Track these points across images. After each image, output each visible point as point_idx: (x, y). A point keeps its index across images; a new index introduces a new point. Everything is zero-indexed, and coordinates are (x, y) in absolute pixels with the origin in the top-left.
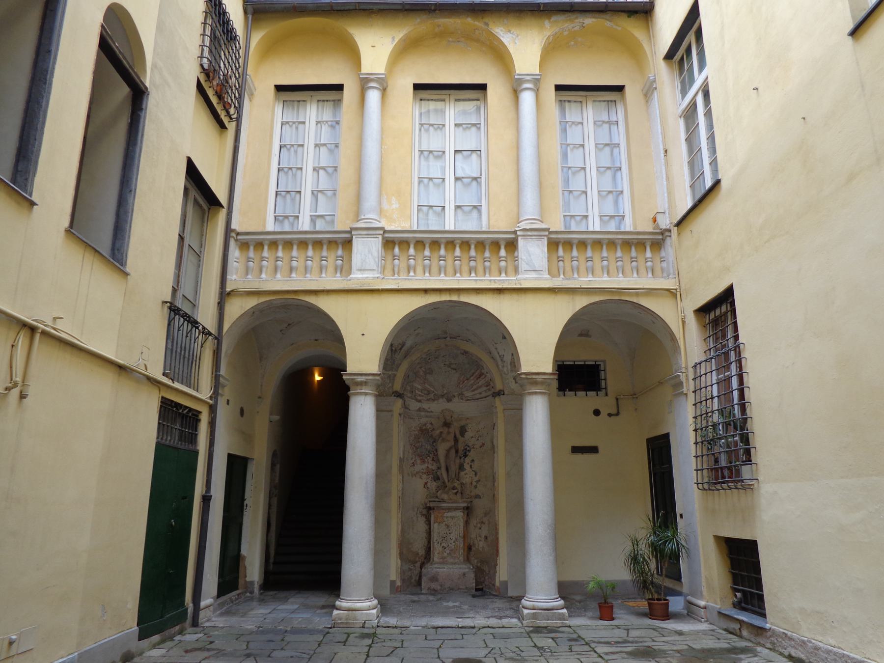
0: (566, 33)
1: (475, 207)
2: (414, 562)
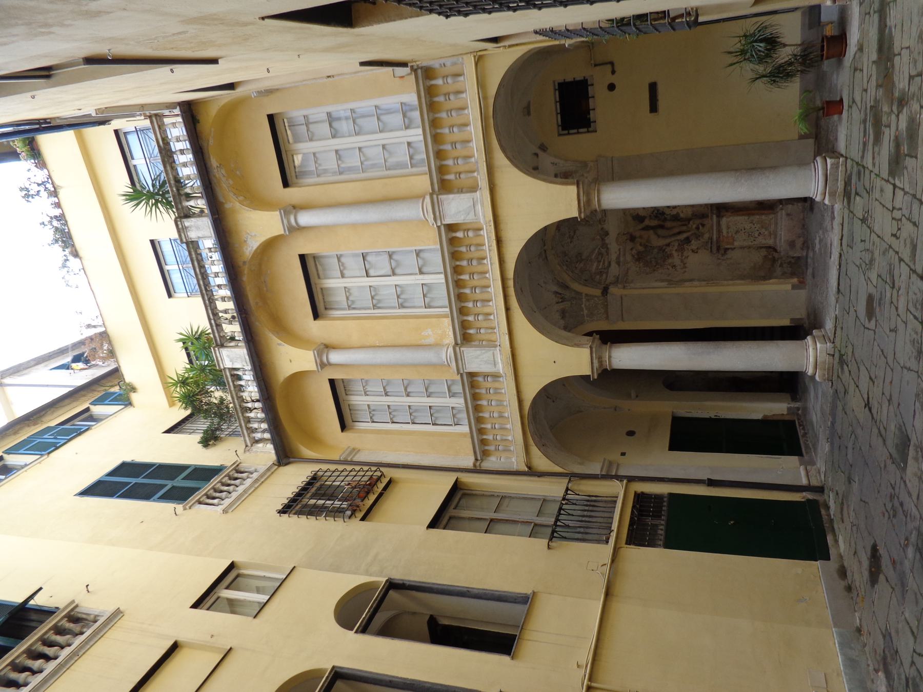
0: (231, 182)
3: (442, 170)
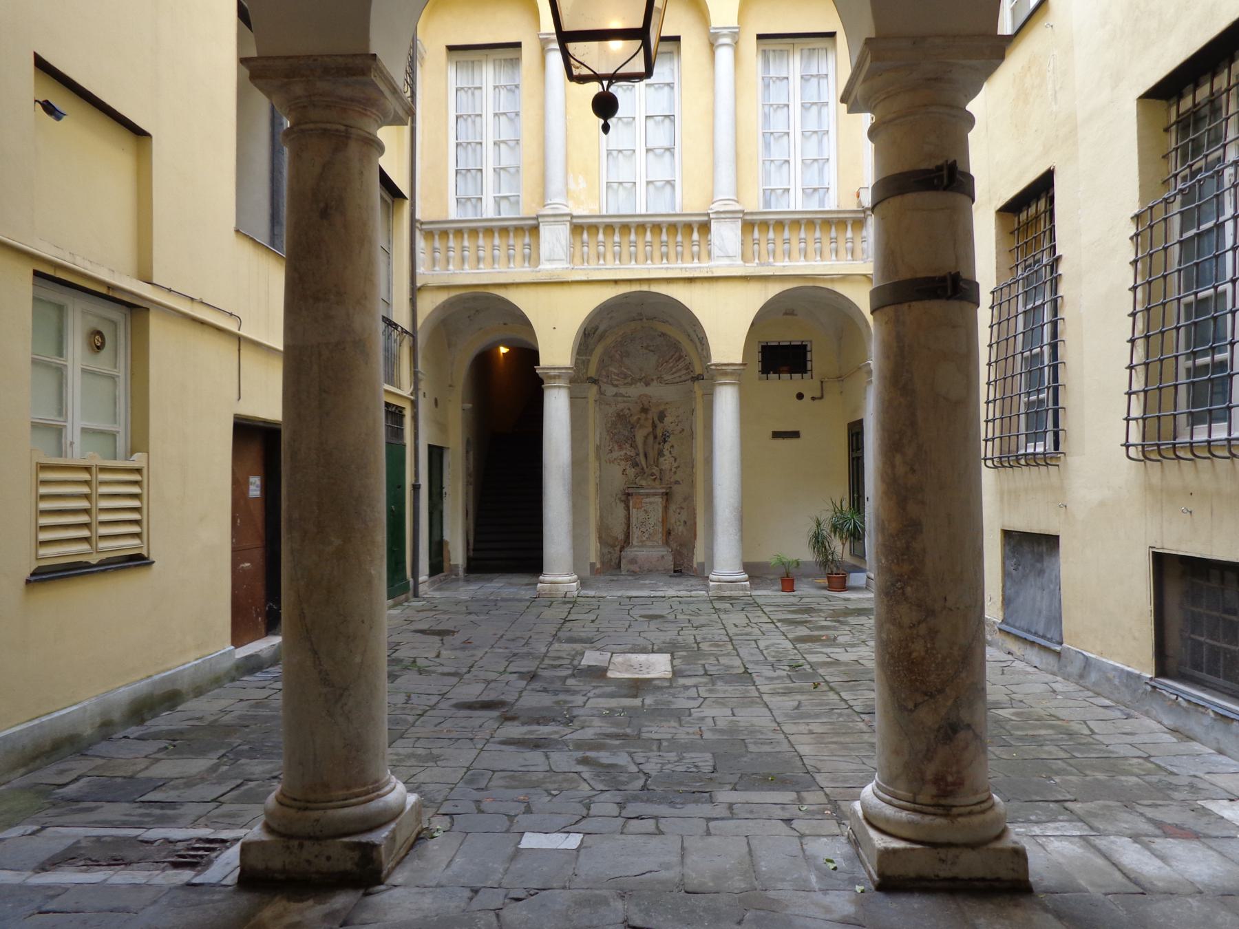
1: (668, 182)
2: (613, 546)
3: (764, 225)
